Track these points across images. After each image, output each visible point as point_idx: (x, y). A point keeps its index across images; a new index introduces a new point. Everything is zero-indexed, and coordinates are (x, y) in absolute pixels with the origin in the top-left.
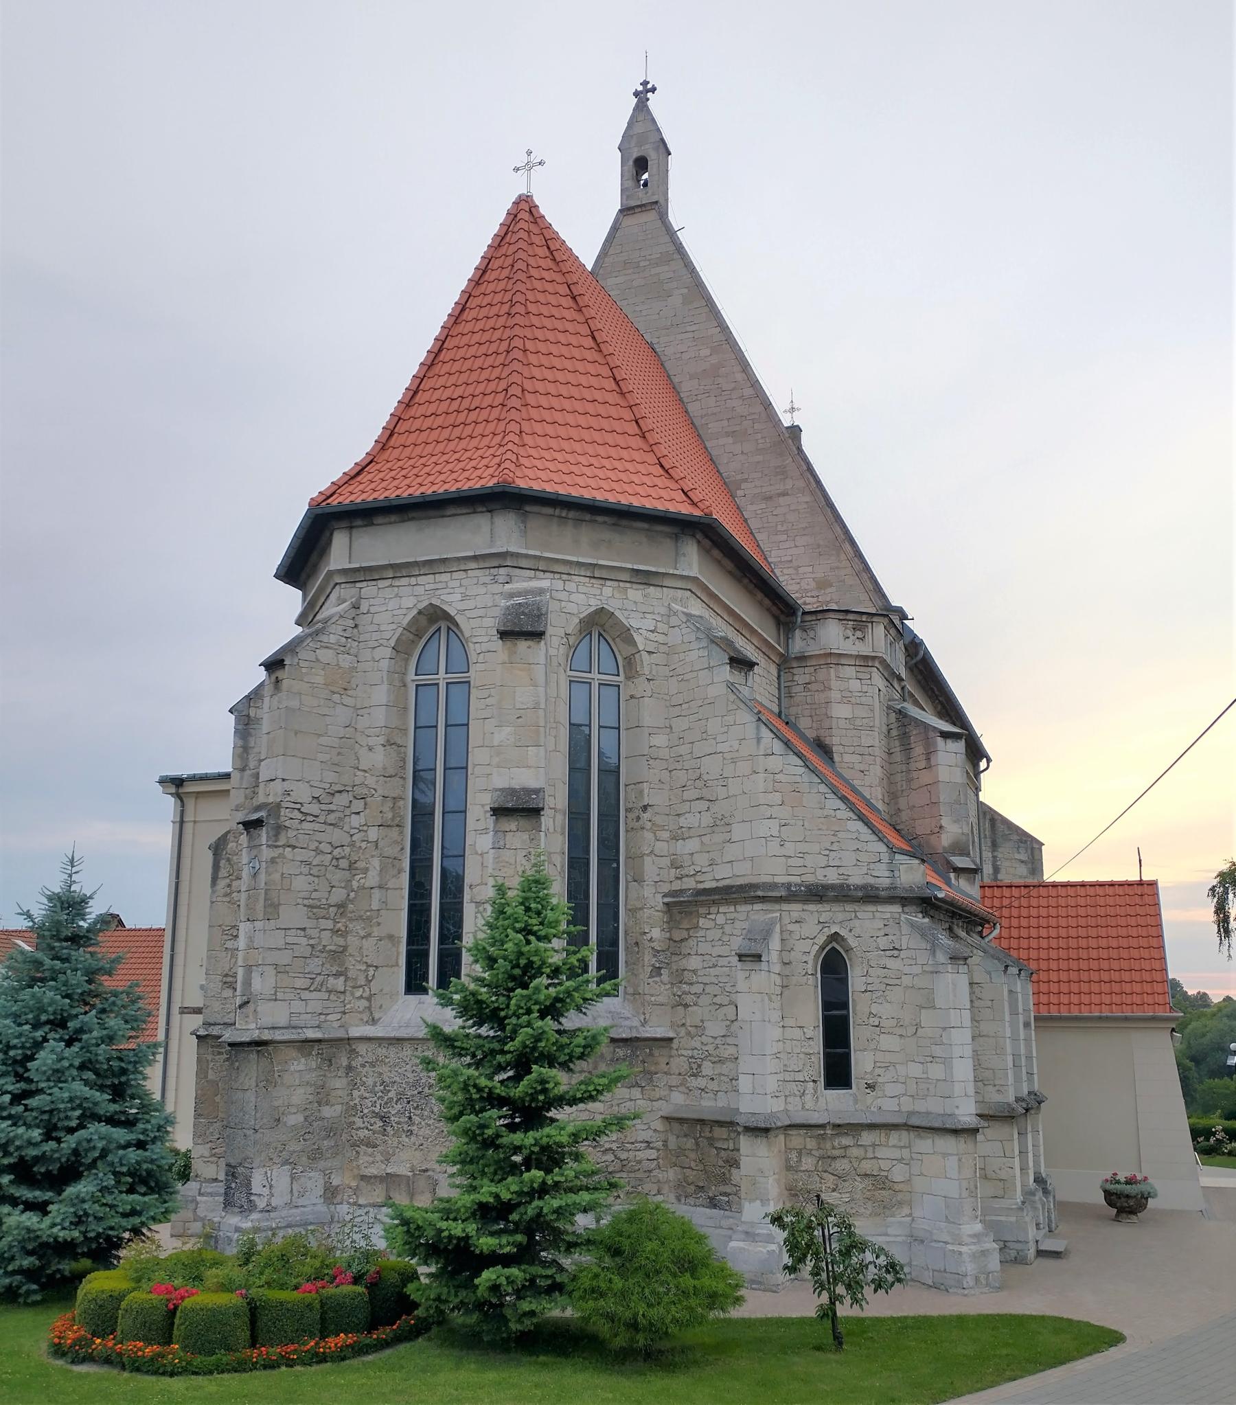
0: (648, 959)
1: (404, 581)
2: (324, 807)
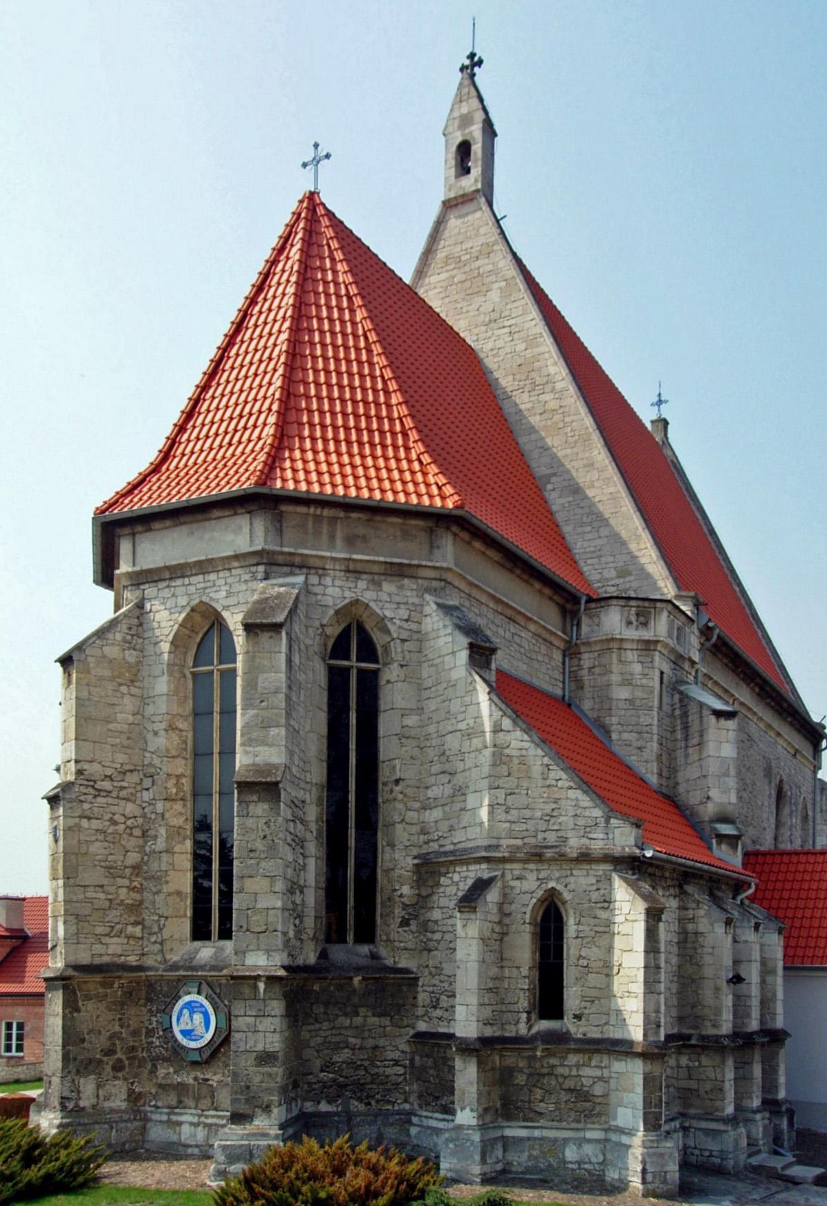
0: (398, 912)
1: (179, 582)
2: (116, 784)
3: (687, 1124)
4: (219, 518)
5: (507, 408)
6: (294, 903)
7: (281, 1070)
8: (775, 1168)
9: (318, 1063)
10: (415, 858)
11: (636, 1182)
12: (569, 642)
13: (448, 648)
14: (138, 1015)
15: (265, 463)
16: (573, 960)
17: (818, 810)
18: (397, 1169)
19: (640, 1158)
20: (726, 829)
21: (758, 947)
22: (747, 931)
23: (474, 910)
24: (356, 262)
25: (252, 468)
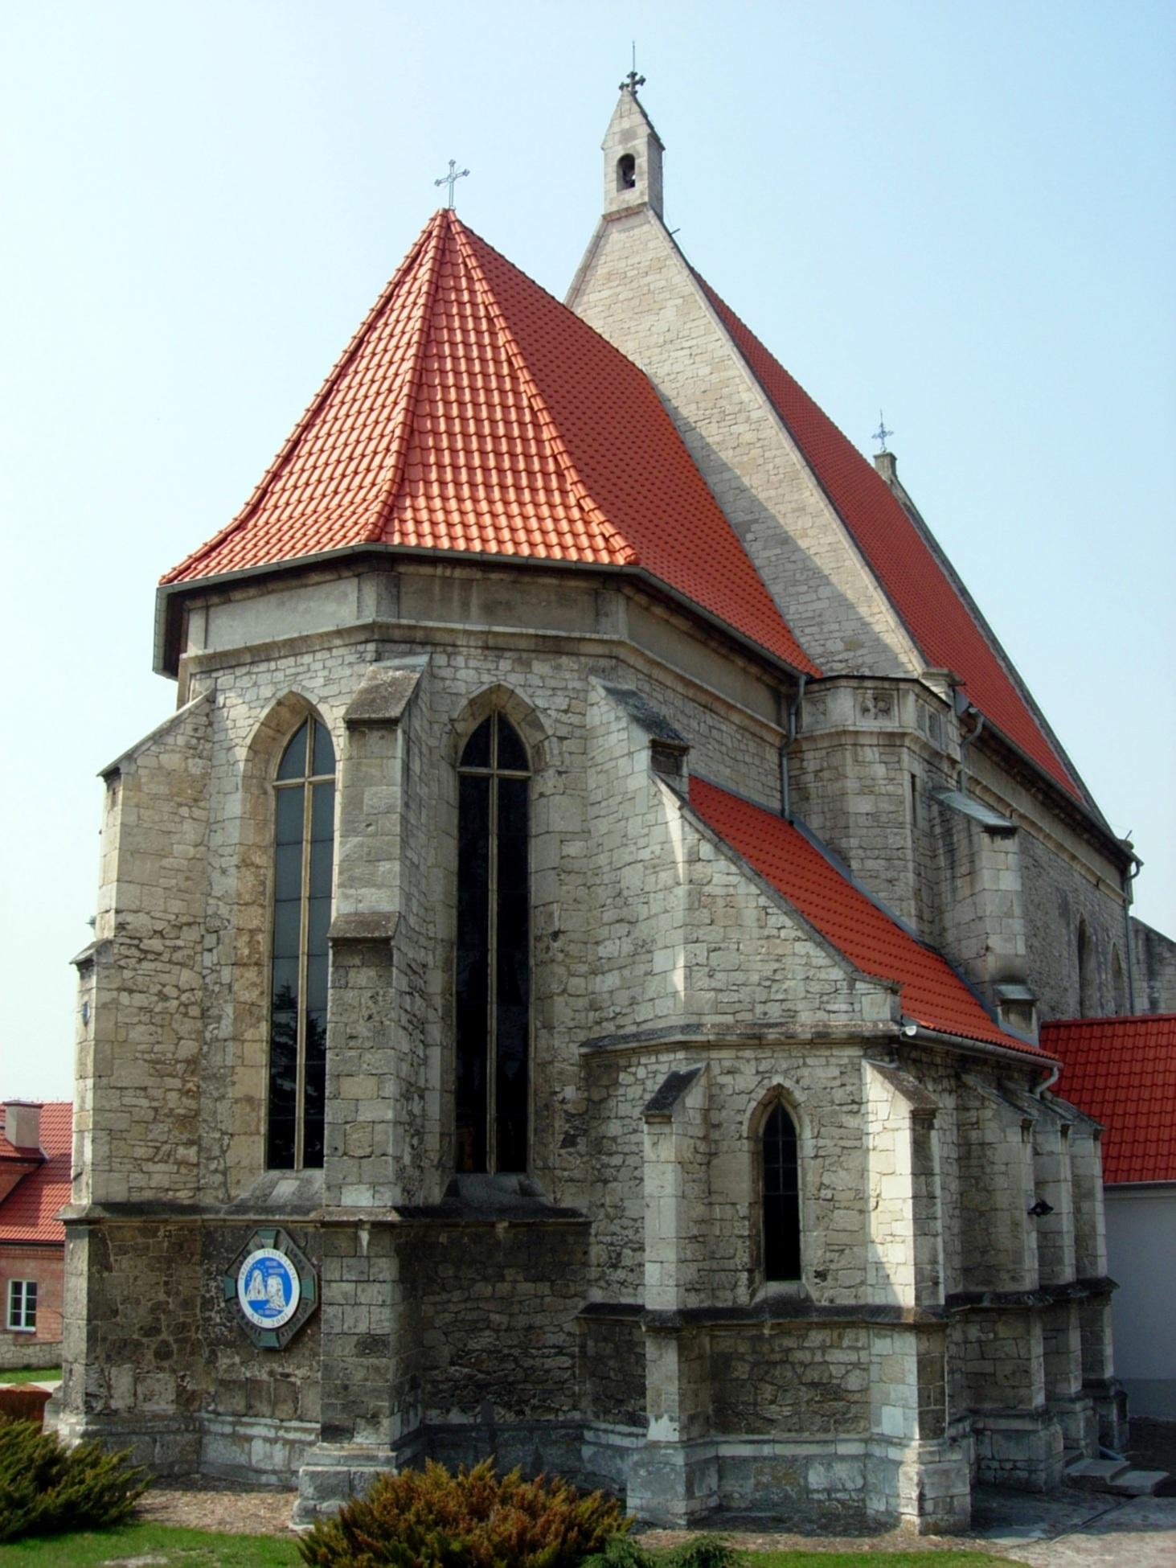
0: (560, 1125)
1: (263, 667)
2: (168, 943)
3: (980, 1425)
4: (318, 583)
5: (691, 442)
6: (410, 1113)
7: (394, 1361)
8: (1102, 1478)
9: (446, 1352)
10: (582, 1045)
11: (910, 1514)
12: (786, 737)
13: (623, 749)
14: (191, 1278)
15: (380, 514)
16: (811, 1190)
17: (1134, 960)
18: (564, 1508)
19: (916, 1479)
20: (1014, 992)
21: (1067, 1160)
22: (1052, 1138)
23: (668, 1120)
24: (497, 281)
25: (362, 521)
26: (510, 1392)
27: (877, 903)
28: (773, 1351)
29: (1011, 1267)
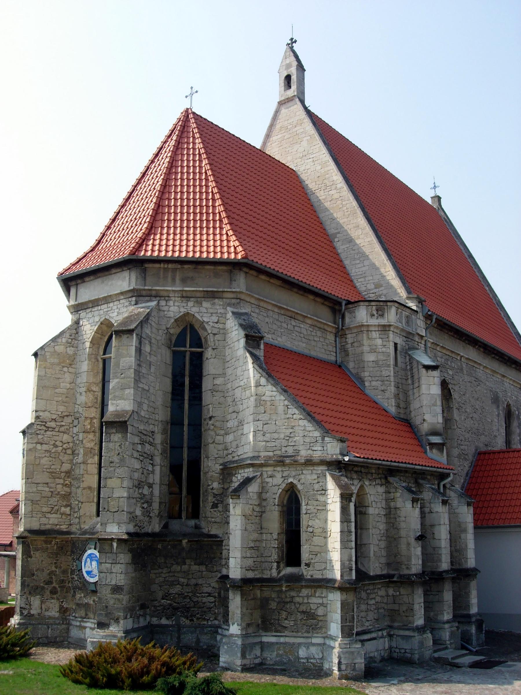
0: (211, 499)
1: (96, 308)
2: (58, 424)
3: (392, 633)
5: (312, 198)
8: (448, 658)
9: (160, 594)
13: (236, 337)
14: (65, 561)
19: (337, 655)
23: (238, 497)
26: (188, 612)
27: (377, 401)
28: (286, 597)
29: (406, 563)
